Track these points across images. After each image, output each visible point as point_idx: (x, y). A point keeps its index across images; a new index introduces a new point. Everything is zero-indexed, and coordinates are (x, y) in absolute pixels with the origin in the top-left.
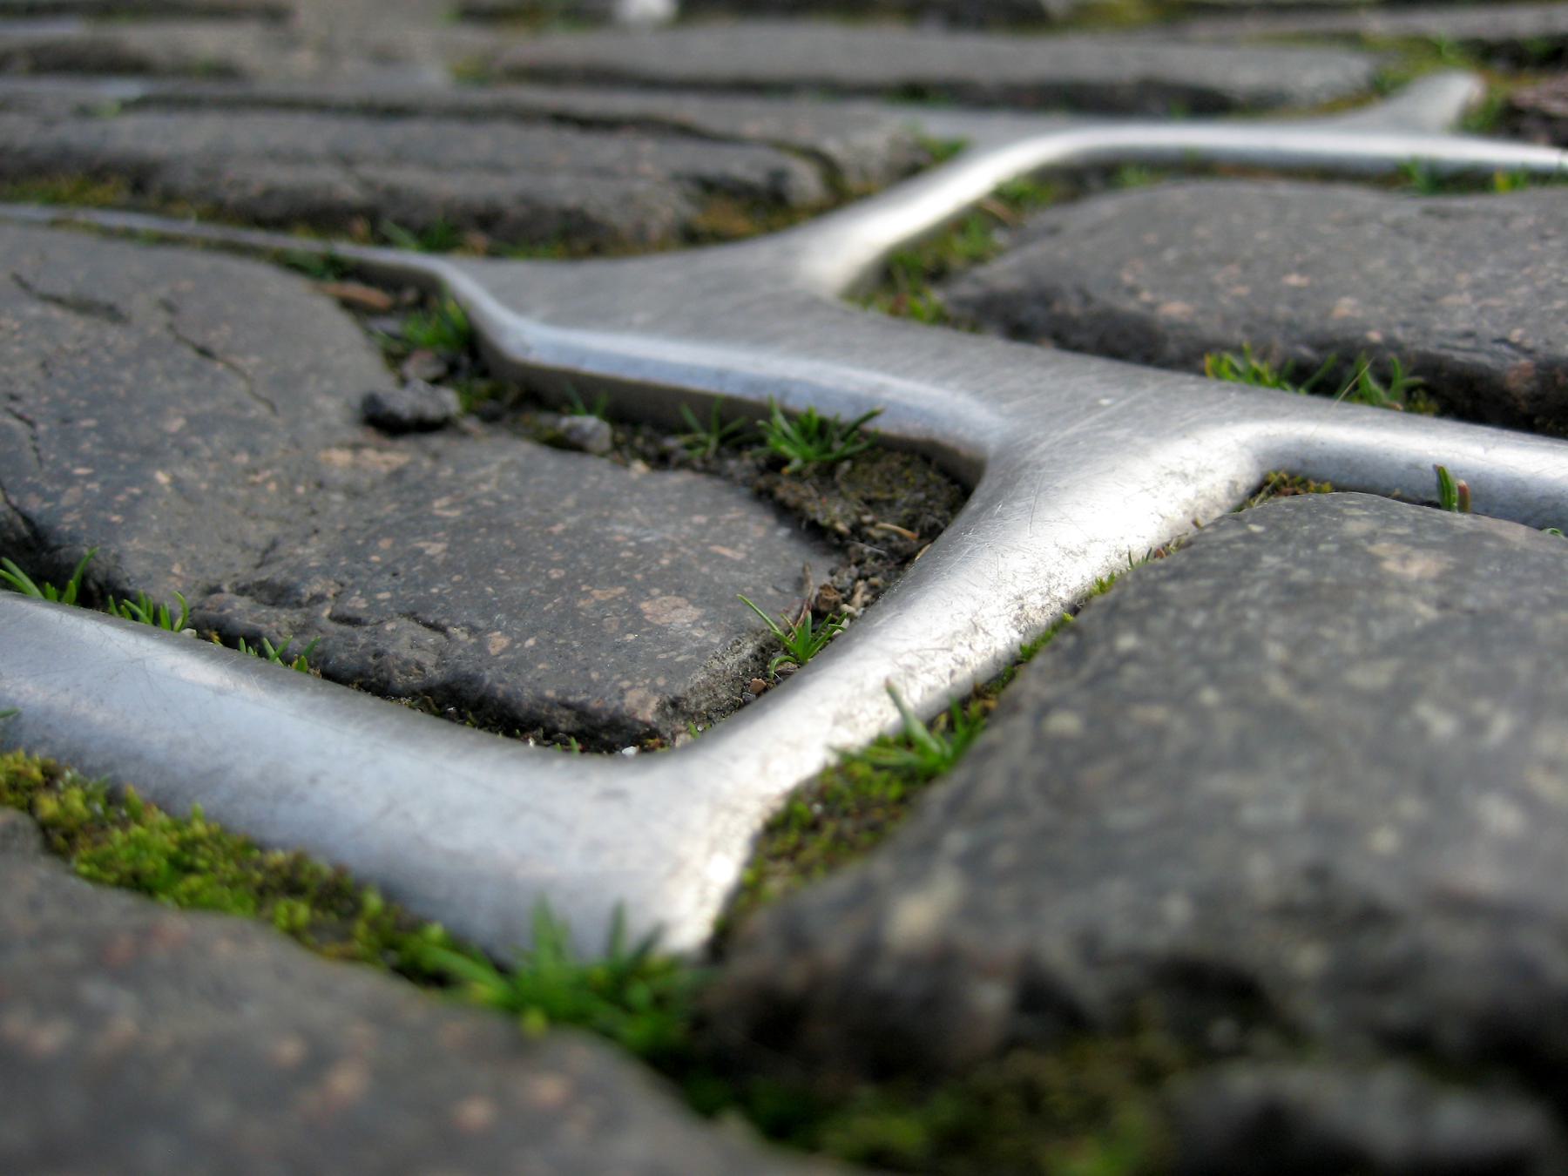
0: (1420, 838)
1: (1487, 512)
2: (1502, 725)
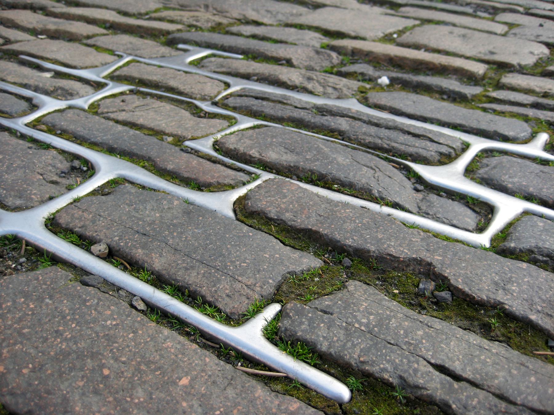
0: (543, 244)
1: (387, 205)
2: (548, 238)
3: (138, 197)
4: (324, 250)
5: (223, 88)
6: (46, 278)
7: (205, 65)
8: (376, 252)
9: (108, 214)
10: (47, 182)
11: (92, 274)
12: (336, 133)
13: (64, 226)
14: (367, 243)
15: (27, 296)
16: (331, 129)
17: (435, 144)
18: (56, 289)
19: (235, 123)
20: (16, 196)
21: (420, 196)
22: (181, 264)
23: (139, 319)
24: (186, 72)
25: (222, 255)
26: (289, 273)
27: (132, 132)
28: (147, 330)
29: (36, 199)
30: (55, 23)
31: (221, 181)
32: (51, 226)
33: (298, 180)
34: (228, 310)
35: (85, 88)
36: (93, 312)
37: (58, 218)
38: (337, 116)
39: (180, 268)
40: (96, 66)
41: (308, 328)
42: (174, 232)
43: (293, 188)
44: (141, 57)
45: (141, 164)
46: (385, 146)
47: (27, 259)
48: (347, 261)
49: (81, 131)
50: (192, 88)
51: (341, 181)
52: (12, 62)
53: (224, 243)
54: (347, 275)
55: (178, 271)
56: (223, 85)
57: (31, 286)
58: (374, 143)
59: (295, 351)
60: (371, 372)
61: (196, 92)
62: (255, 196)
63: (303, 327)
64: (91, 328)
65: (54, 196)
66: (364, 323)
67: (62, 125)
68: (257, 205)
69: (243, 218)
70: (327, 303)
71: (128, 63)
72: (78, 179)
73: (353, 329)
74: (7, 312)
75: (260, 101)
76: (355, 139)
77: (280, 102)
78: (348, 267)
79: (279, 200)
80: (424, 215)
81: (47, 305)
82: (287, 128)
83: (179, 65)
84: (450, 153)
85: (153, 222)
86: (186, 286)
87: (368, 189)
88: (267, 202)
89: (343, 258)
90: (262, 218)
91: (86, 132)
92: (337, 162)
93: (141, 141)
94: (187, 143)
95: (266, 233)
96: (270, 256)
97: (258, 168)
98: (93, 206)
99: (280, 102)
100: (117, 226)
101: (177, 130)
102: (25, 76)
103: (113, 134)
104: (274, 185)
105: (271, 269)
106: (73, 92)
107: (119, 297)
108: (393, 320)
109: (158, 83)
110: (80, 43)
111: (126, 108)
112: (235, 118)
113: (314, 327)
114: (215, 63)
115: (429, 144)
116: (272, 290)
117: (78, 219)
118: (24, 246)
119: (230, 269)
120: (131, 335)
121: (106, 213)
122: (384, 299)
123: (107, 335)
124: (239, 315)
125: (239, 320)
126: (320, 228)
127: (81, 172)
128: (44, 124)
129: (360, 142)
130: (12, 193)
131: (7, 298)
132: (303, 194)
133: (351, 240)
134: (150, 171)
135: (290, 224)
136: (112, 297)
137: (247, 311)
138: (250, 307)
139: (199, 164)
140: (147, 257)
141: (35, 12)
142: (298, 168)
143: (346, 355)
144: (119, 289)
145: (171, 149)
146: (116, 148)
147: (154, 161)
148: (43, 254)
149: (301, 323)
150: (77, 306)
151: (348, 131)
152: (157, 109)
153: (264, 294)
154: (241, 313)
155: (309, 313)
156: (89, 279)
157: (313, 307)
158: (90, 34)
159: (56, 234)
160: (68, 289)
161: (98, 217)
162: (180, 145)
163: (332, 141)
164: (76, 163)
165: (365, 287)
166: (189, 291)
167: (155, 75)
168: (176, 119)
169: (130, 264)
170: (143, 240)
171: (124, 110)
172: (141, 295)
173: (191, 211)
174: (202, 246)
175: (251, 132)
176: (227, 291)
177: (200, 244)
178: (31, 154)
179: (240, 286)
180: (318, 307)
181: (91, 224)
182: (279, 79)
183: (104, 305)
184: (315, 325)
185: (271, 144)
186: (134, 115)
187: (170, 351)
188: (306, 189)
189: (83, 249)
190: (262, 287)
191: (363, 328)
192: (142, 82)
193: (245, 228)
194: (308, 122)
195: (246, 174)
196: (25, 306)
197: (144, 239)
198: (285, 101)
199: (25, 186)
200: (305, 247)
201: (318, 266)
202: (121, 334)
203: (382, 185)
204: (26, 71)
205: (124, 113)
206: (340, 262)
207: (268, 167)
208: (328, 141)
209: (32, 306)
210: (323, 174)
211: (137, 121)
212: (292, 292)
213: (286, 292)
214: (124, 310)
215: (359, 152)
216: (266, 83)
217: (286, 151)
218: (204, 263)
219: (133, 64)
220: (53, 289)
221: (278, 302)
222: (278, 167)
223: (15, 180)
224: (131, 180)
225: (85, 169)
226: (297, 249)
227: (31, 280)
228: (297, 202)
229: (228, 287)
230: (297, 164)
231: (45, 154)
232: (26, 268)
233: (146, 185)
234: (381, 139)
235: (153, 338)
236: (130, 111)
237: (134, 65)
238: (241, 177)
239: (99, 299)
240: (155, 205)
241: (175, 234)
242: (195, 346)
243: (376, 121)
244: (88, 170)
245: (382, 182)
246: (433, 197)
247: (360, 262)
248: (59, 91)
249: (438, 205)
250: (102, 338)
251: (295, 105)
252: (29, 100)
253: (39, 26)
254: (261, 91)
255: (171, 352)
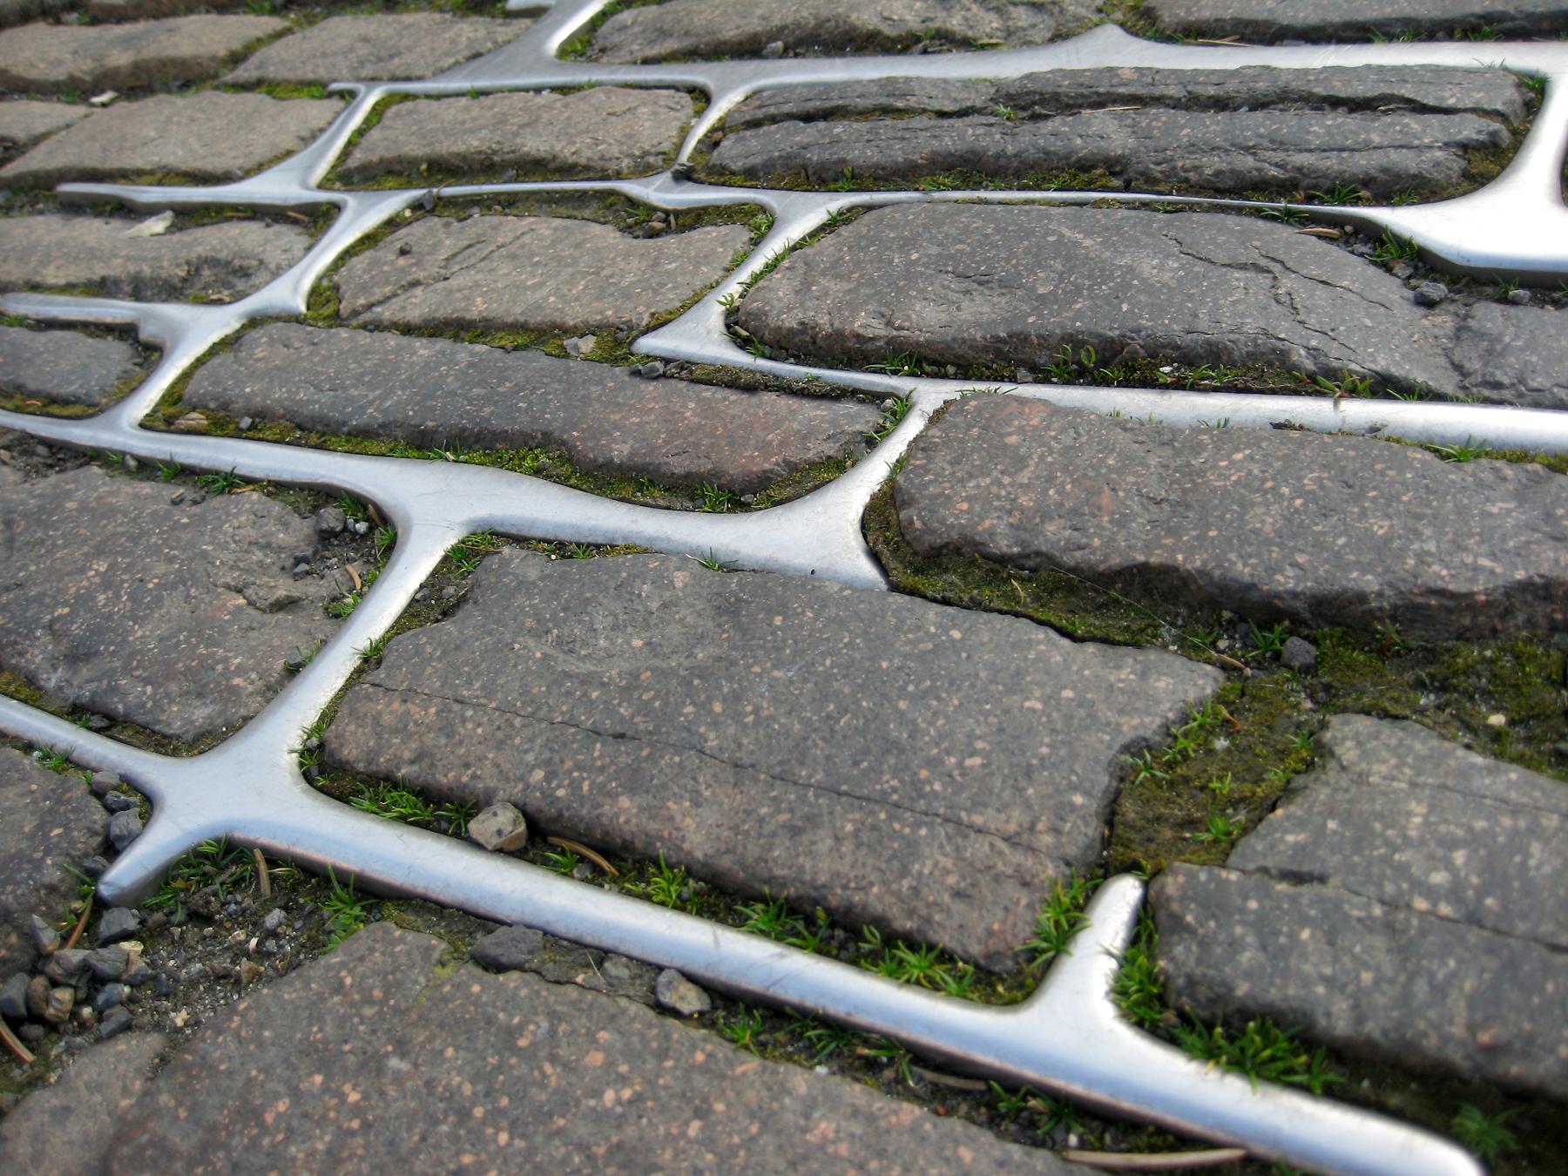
1: (1353, 392)
3: (556, 594)
4: (1209, 626)
5: (690, 111)
6: (364, 977)
7: (608, 44)
8: (1388, 592)
9: (483, 688)
10: (264, 611)
11: (502, 923)
12: (1099, 171)
13: (361, 767)
14: (1347, 567)
15: (325, 1058)
16: (1079, 160)
17: (1435, 119)
18: (408, 1009)
19: (770, 226)
20: (187, 693)
21: (1443, 321)
22: (772, 816)
23: (700, 1057)
24: (563, 90)
25: (891, 746)
26: (1126, 749)
27: (467, 352)
28: (738, 1094)
29: (250, 688)
30: (126, 42)
31: (795, 455)
32: (321, 774)
33: (1036, 381)
34: (975, 949)
35: (278, 236)
36: (548, 1068)
37: (333, 745)
38: (1081, 106)
39: (774, 834)
40: (289, 154)
41: (1262, 957)
42: (710, 700)
43: (1035, 422)
44: (408, 79)
45: (528, 463)
46: (1274, 172)
47: (285, 908)
48: (1299, 650)
49: (312, 400)
50: (597, 142)
51: (1179, 348)
52: (41, 213)
53: (884, 696)
54: (1312, 697)
55: (771, 848)
56: (686, 99)
57: (328, 1017)
58: (1233, 171)
59: (1242, 1050)
60: (1534, 1081)
61: (615, 151)
62: (925, 486)
63: (1246, 957)
64: (559, 1132)
65: (298, 660)
66: (1439, 886)
67: (249, 397)
68: (942, 522)
69: (910, 580)
70: (1290, 838)
71: (378, 111)
72: (349, 567)
73: (1415, 922)
74: (286, 1138)
75: (822, 125)
76: (1167, 176)
77: (886, 111)
78: (1307, 670)
79: (1006, 480)
80: (1486, 392)
81: (398, 1079)
82: (936, 195)
83: (530, 70)
84: (1493, 134)
85: (632, 685)
86: (813, 893)
87: (1274, 351)
88: (968, 499)
89: (1283, 642)
90: (972, 563)
91: (326, 398)
92: (1143, 281)
93: (502, 380)
94: (648, 343)
95: (1001, 612)
96: (1045, 703)
97: (895, 373)
98: (429, 670)
99: (886, 111)
100: (524, 726)
101: (598, 305)
102: (93, 254)
103: (411, 382)
104: (970, 427)
105: (1063, 752)
106: (245, 263)
107: (613, 987)
108: (1536, 848)
109: (488, 157)
110: (216, 88)
111: (421, 275)
112: (763, 209)
113: (1282, 949)
114: (636, 29)
115: (1413, 123)
116: (1092, 830)
117: (396, 731)
118: (263, 867)
119: (935, 794)
120: (694, 1128)
121: (477, 685)
122: (1473, 766)
123: (620, 1146)
124: (1016, 956)
125: (1020, 972)
126: (1174, 551)
127: (353, 540)
128: (194, 409)
129: (1187, 180)
130: (173, 688)
131: (270, 1086)
132: (1072, 432)
133: (1290, 572)
134: (562, 481)
135: (1072, 563)
136: (590, 996)
137: (1037, 934)
138: (1042, 917)
139: (706, 409)
140: (653, 818)
141: (58, 22)
142: (1023, 338)
143: (1425, 1034)
144: (602, 955)
145: (601, 382)
146: (435, 431)
147: (564, 443)
148: (328, 880)
149: (1235, 945)
150: (493, 1060)
151: (1135, 152)
152: (512, 248)
153: (1072, 851)
154: (1018, 947)
155: (1246, 898)
156: (499, 945)
157: (1251, 866)
158: (237, 46)
159: (348, 802)
160: (446, 1000)
161: (456, 707)
162: (625, 359)
163: (1096, 204)
164: (331, 517)
165: (1386, 727)
166: (828, 911)
167: (472, 131)
168: (582, 266)
169: (606, 853)
170: (624, 760)
171: (415, 284)
172: (678, 963)
173: (738, 600)
174: (816, 730)
175: (828, 241)
176: (951, 880)
177: (807, 723)
178: (185, 526)
179: (987, 848)
180: (1269, 863)
181: (443, 741)
182: (854, 28)
183: (574, 1032)
184: (1282, 940)
185: (910, 275)
186: (451, 291)
187: (836, 1157)
188: (1078, 412)
189: (445, 832)
190: (1056, 831)
191: (1445, 909)
192: (442, 169)
193: (931, 615)
194: (998, 156)
195: (862, 401)
196: (334, 1102)
197: (625, 755)
198: (900, 104)
199: (202, 650)
200: (1142, 630)
201: (1209, 691)
202: (662, 1130)
203: (1312, 321)
204: (92, 231)
205: (418, 291)
206: (1277, 656)
207: (926, 359)
208: (1081, 204)
209: (354, 1097)
210: (1112, 340)
211: (467, 309)
212: (1159, 819)
213: (1140, 823)
214: (642, 1037)
215: (1195, 217)
216: (817, 55)
217: (965, 285)
218: (846, 794)
219: (394, 109)
220: (397, 1011)
221: (1131, 868)
222: (960, 351)
223: (168, 638)
224: (514, 531)
225: (362, 527)
226: (1118, 644)
227: (321, 998)
228: (1065, 470)
229: (948, 863)
230: (1017, 328)
231: (228, 514)
232: (293, 939)
233: (564, 536)
234: (1249, 150)
235: (767, 1119)
236: (436, 280)
237: (398, 115)
238: (852, 418)
239: (553, 1016)
240: (617, 607)
241: (718, 707)
242: (910, 1112)
243: (1211, 91)
244: (371, 529)
245: (1309, 311)
246: (1489, 315)
247: (1343, 642)
248: (206, 272)
249: (1520, 343)
250: (607, 1165)
251: (936, 105)
252: (126, 332)
253: (83, 67)
254: (811, 86)
255: (842, 1159)
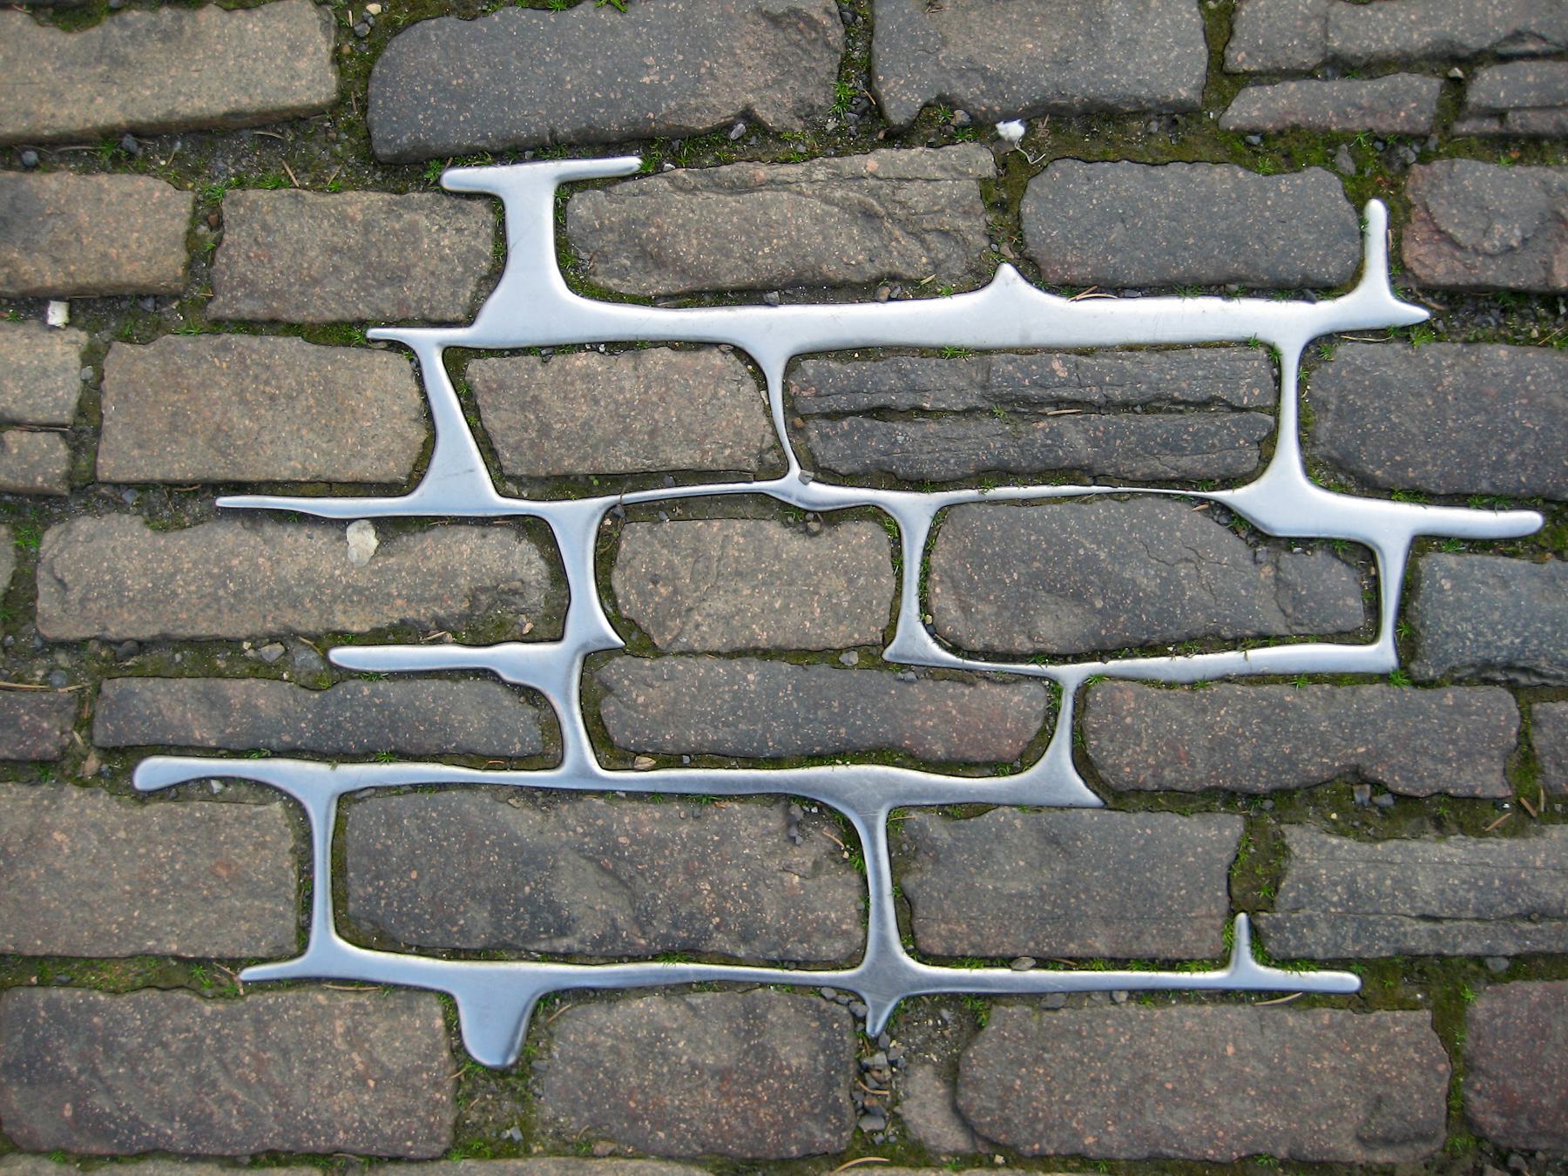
116: (1226, 901)
